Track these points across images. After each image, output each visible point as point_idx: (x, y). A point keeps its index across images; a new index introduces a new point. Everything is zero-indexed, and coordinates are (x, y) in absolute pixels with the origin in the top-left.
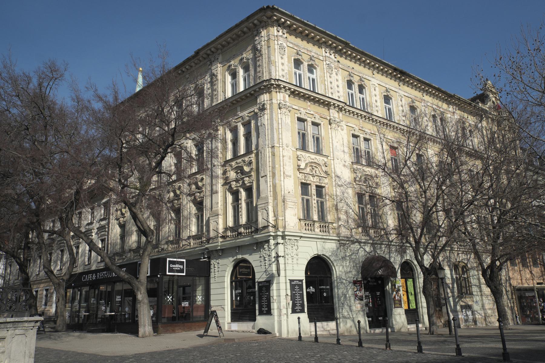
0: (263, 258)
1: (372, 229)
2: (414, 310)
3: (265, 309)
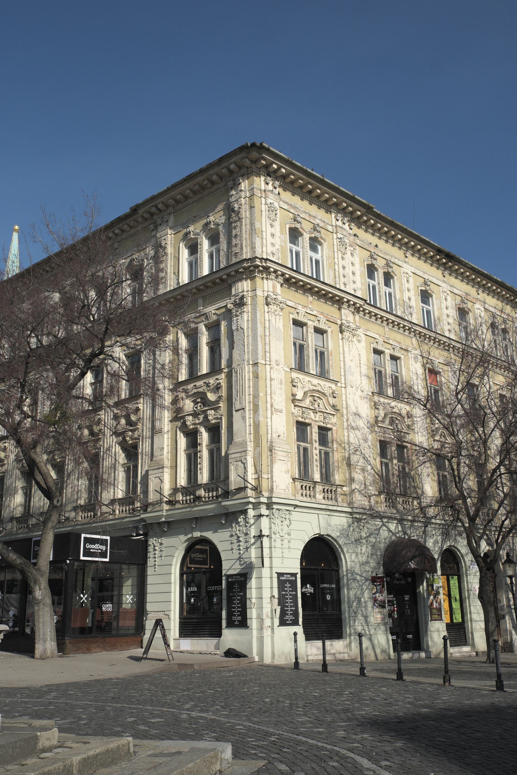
0: (235, 537)
1: (400, 498)
2: (459, 624)
3: (237, 618)
